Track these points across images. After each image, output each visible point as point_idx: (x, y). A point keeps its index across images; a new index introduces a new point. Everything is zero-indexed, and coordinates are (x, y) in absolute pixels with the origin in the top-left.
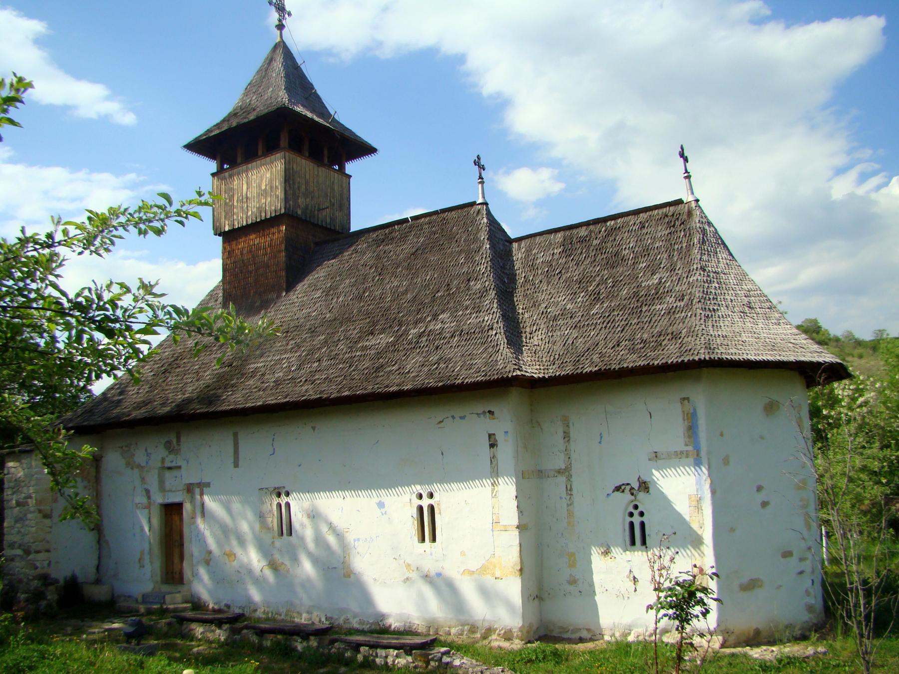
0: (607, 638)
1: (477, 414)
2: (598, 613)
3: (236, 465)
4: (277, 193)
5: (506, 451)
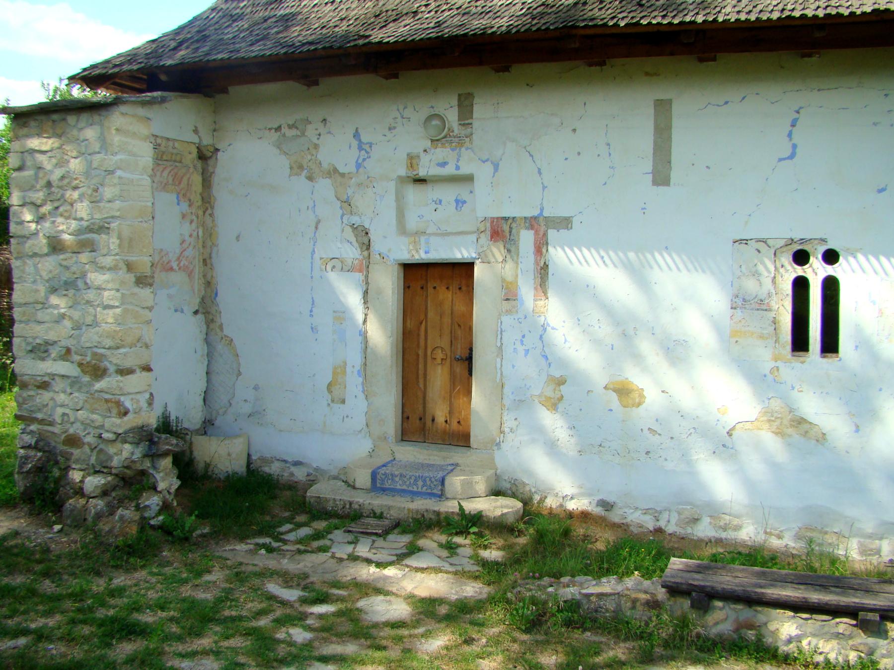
3: (661, 177)
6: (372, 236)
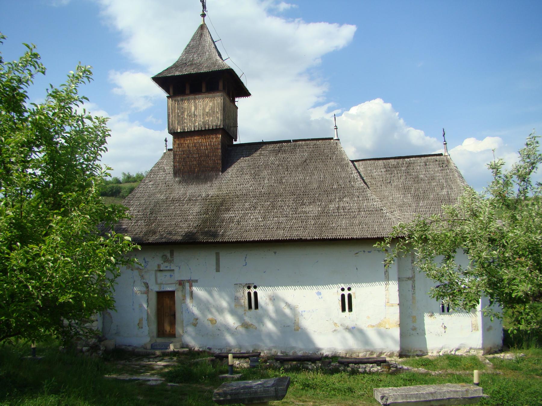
0: (430, 354)
1: (378, 250)
2: (426, 342)
3: (218, 270)
4: (218, 116)
5: (393, 270)
6: (149, 285)
